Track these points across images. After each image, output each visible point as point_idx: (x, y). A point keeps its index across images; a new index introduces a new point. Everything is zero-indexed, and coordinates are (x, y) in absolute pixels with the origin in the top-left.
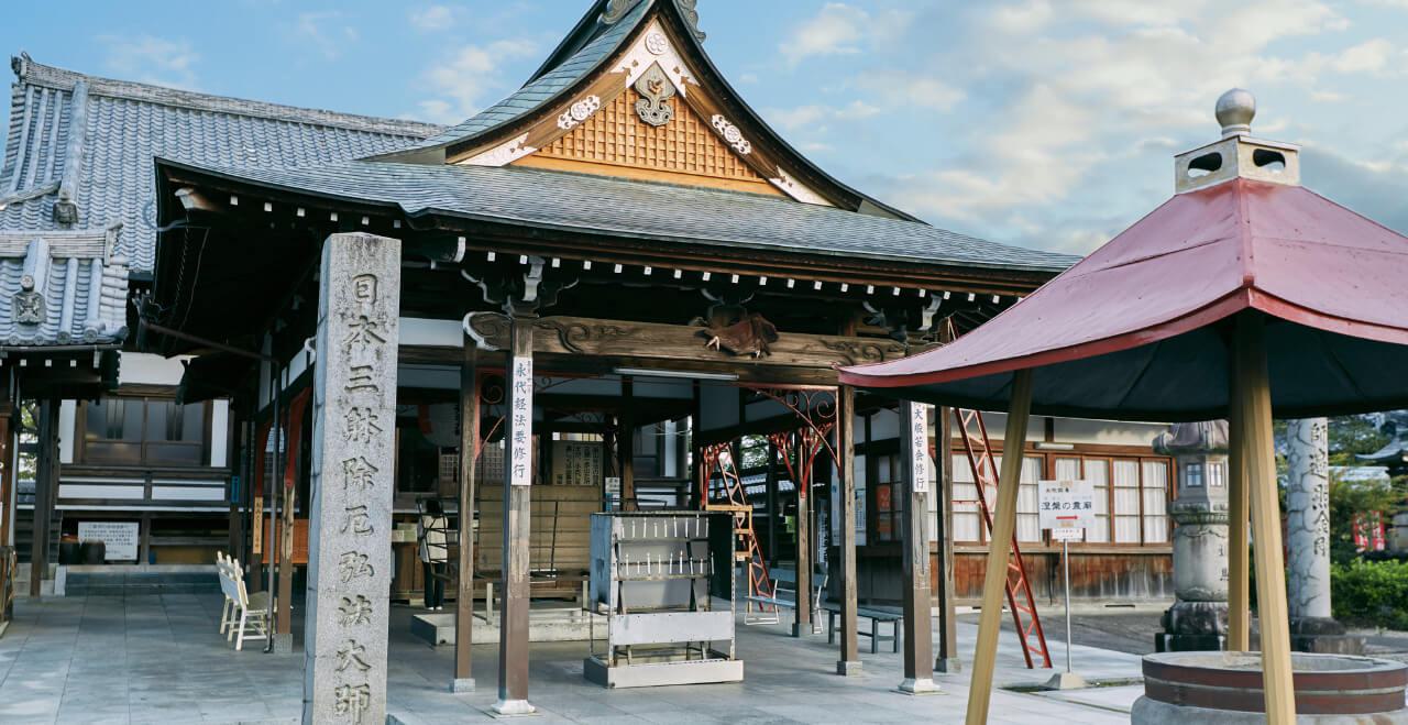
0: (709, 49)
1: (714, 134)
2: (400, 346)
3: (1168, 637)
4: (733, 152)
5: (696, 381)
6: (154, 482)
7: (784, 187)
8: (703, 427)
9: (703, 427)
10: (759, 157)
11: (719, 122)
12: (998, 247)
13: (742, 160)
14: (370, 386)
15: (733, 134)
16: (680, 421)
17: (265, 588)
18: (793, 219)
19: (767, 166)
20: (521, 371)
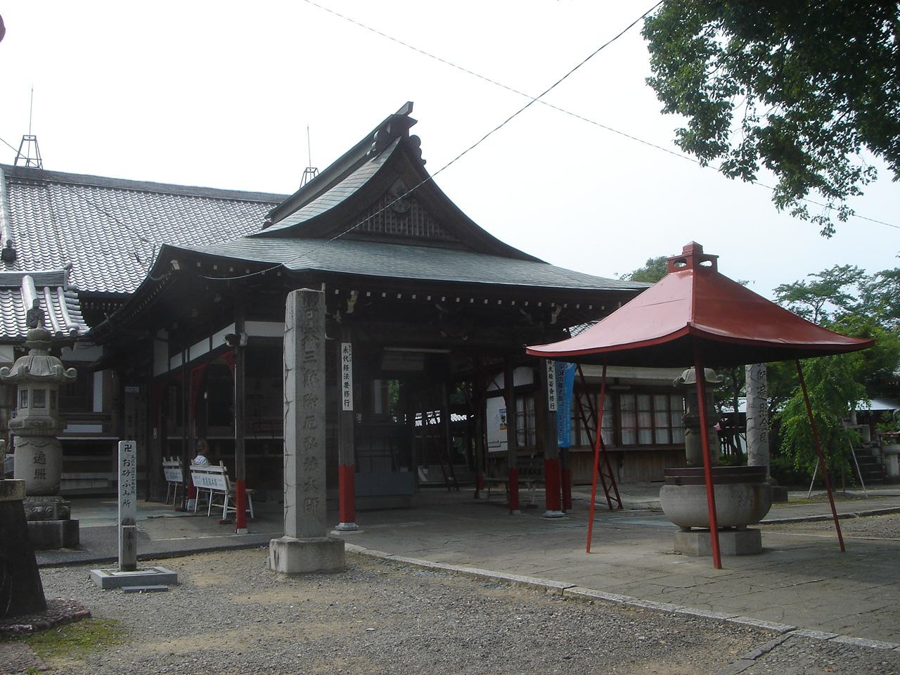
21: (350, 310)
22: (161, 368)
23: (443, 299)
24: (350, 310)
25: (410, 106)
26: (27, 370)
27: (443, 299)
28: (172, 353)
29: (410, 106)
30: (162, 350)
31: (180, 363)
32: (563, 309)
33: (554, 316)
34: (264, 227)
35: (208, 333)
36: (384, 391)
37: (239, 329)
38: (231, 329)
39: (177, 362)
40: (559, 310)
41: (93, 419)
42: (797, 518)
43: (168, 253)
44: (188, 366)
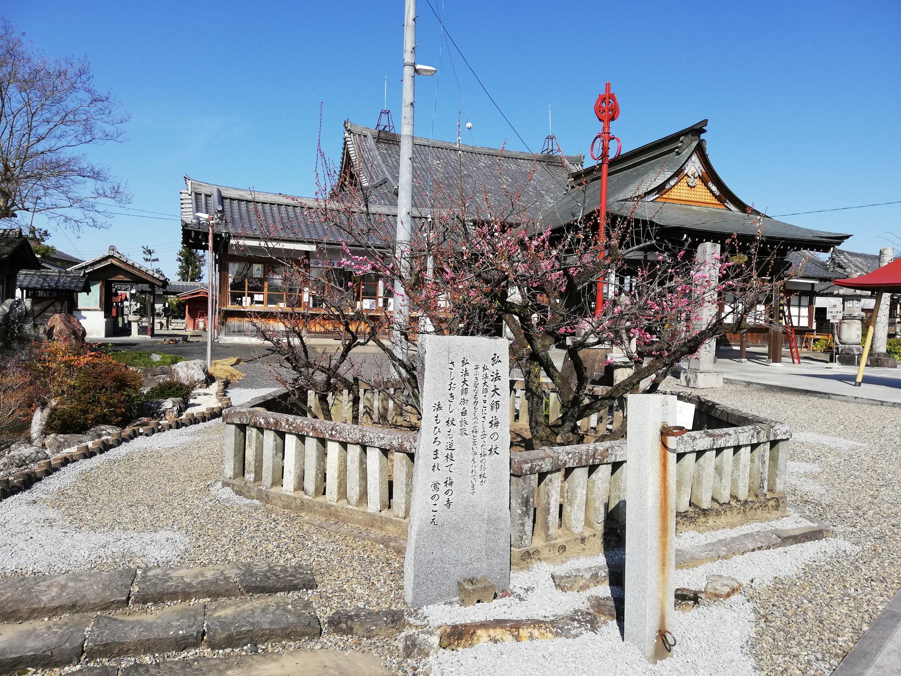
1: (709, 188)
4: (714, 194)
11: (710, 184)
13: (716, 197)
15: (714, 188)
18: (730, 220)
19: (723, 198)
25: (705, 122)
29: (705, 122)
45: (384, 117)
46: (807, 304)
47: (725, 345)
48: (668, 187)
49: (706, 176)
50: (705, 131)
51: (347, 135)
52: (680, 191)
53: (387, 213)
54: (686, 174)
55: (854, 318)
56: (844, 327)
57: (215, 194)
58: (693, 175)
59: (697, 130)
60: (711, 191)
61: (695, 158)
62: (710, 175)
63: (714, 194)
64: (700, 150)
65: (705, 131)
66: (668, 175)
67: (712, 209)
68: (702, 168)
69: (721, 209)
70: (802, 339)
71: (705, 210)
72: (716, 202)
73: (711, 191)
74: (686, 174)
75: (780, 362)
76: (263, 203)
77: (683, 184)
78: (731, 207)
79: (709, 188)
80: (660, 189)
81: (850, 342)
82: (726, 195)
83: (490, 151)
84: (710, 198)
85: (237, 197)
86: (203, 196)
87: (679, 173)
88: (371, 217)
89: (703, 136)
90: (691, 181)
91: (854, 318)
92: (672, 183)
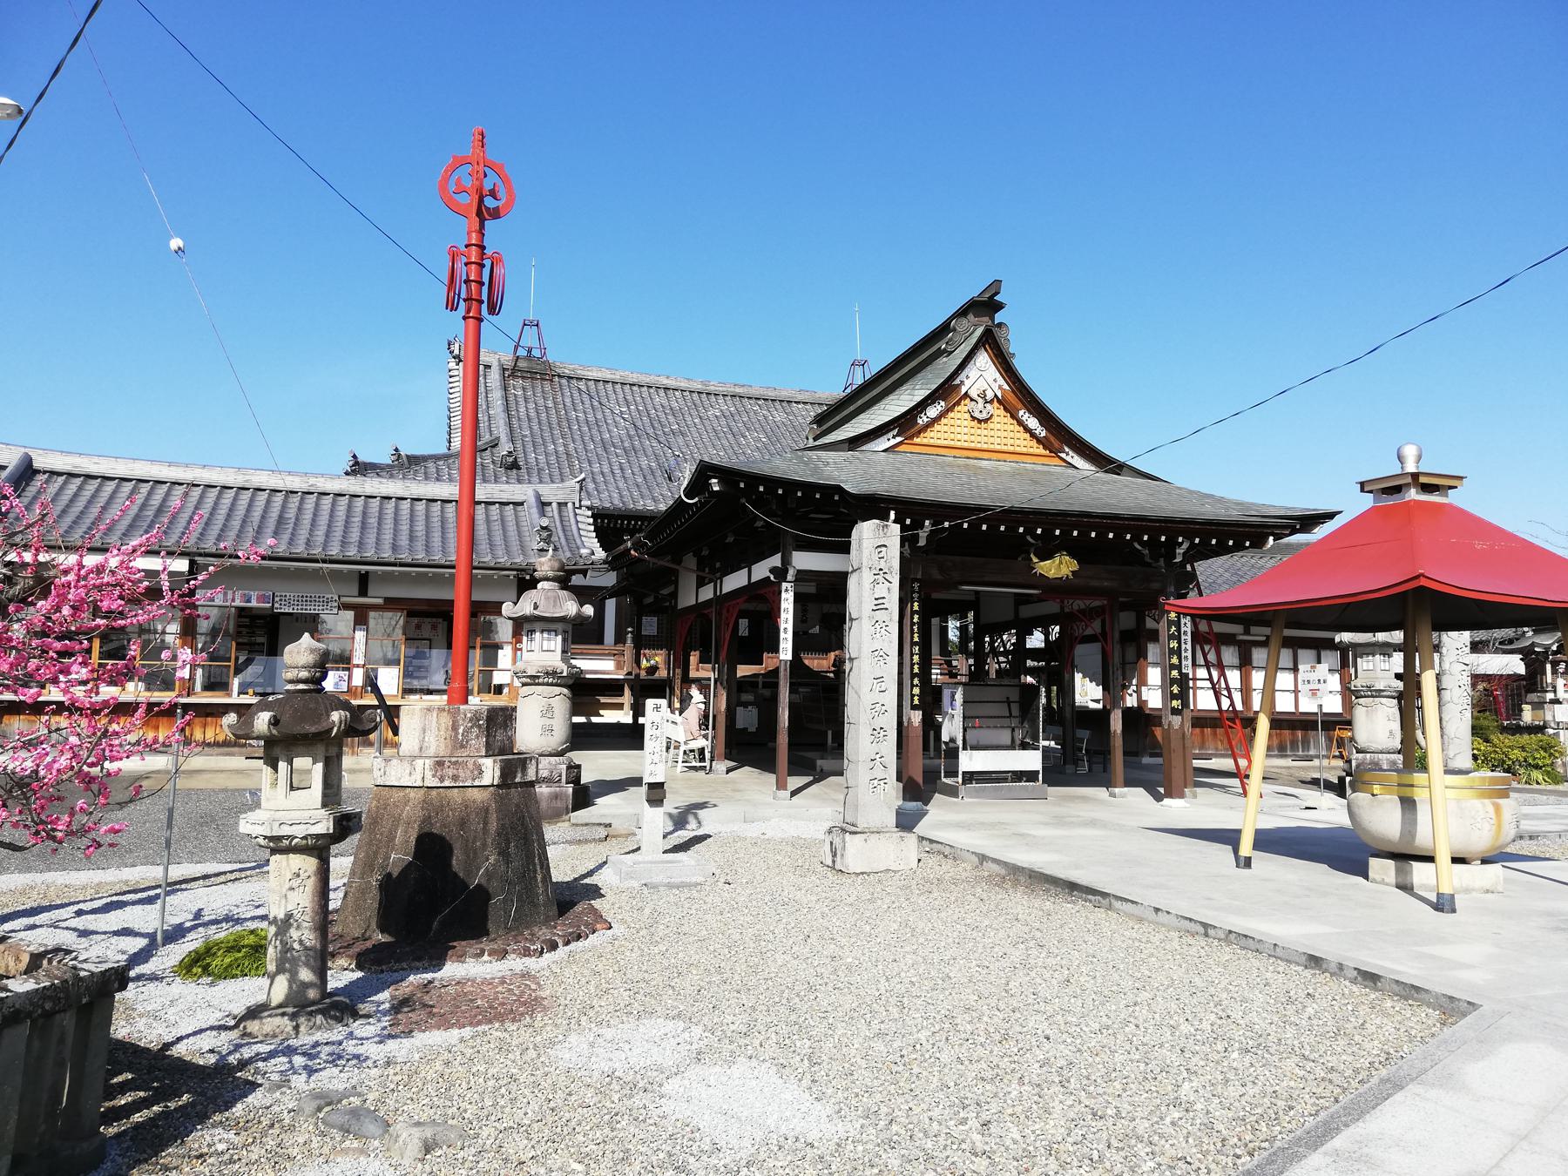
0: (1018, 364)
1: (1020, 423)
2: (640, 747)
3: (1348, 779)
4: (1033, 435)
5: (977, 592)
6: (603, 700)
7: (1068, 459)
8: (983, 621)
9: (983, 621)
10: (1052, 439)
11: (1023, 414)
12: (1221, 500)
13: (1039, 441)
14: (246, 920)
15: (1033, 423)
16: (963, 616)
17: (819, 426)
18: (1075, 486)
19: (1056, 443)
20: (786, 610)
21: (922, 543)
22: (687, 599)
23: (1039, 531)
24: (922, 543)
25: (996, 286)
26: (645, 1084)
27: (1039, 531)
28: (701, 583)
29: (996, 286)
30: (687, 582)
31: (711, 595)
32: (1192, 544)
33: (1180, 551)
34: (815, 439)
35: (749, 562)
36: (944, 631)
37: (786, 562)
38: (776, 561)
39: (707, 593)
40: (1185, 546)
41: (600, 612)
42: (968, 559)
43: (705, 471)
44: (721, 600)
45: (530, 332)
46: (1236, 661)
47: (1152, 755)
48: (922, 420)
49: (1012, 398)
50: (1000, 306)
51: (452, 365)
52: (954, 429)
53: (400, 493)
54: (966, 395)
55: (1378, 694)
56: (1360, 715)
57: (532, 500)
58: (983, 395)
59: (986, 305)
60: (1027, 429)
61: (983, 359)
62: (1022, 397)
63: (1033, 435)
64: (991, 342)
65: (1000, 306)
66: (920, 394)
67: (1029, 465)
68: (1001, 381)
69: (1053, 466)
70: (1330, 739)
71: (1005, 467)
72: (1041, 451)
73: (1027, 429)
74: (966, 395)
75: (1182, 796)
76: (502, 504)
77: (960, 415)
78: (1077, 461)
79: (1020, 423)
80: (905, 424)
81: (1374, 746)
82: (1059, 436)
83: (738, 390)
84: (1024, 443)
85: (68, 468)
86: (554, 505)
87: (947, 391)
88: (480, 509)
89: (998, 318)
90: (979, 409)
91: (1378, 694)
92: (933, 412)
